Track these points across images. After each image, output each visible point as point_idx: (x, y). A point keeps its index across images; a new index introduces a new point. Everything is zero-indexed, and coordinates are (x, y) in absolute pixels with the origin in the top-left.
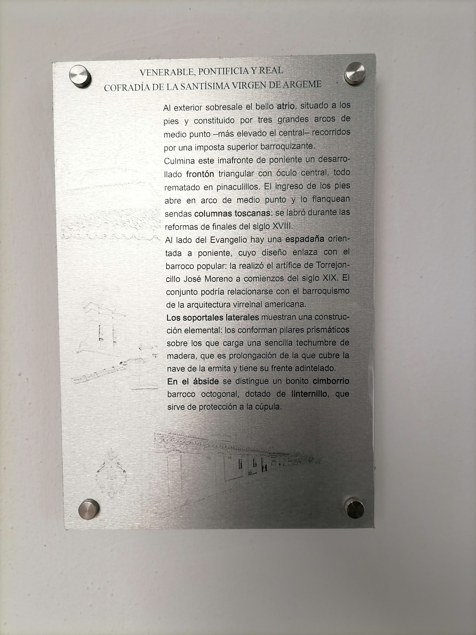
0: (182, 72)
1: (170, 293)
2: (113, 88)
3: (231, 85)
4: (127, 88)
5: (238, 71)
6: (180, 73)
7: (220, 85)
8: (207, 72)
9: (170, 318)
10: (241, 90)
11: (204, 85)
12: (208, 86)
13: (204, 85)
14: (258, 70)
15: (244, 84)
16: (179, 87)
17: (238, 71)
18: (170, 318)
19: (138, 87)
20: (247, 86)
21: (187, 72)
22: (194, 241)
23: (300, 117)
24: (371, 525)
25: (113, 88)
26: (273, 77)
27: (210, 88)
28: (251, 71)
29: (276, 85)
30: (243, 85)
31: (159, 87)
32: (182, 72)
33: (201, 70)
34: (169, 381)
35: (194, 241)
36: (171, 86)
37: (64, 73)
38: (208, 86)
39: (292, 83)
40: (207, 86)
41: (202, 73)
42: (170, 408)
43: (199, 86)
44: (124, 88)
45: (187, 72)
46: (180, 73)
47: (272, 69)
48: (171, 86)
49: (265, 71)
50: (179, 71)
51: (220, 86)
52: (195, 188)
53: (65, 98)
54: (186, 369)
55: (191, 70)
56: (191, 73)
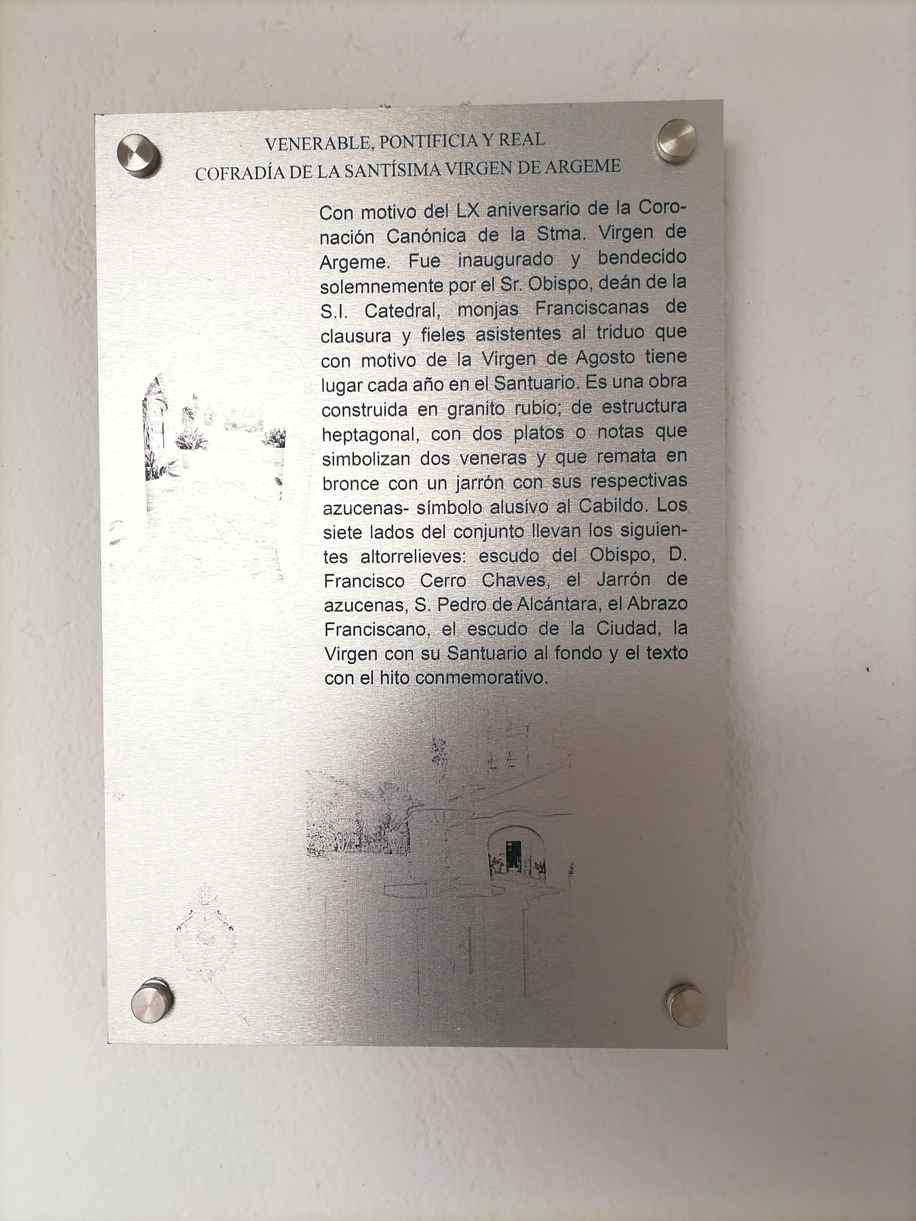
2: (213, 174)
4: (240, 175)
5: (456, 141)
11: (390, 170)
13: (390, 170)
14: (495, 140)
16: (342, 172)
17: (456, 141)
19: (261, 173)
21: (357, 142)
25: (213, 174)
29: (532, 167)
30: (467, 168)
31: (303, 172)
43: (381, 170)
44: (235, 174)
47: (523, 137)
51: (423, 170)
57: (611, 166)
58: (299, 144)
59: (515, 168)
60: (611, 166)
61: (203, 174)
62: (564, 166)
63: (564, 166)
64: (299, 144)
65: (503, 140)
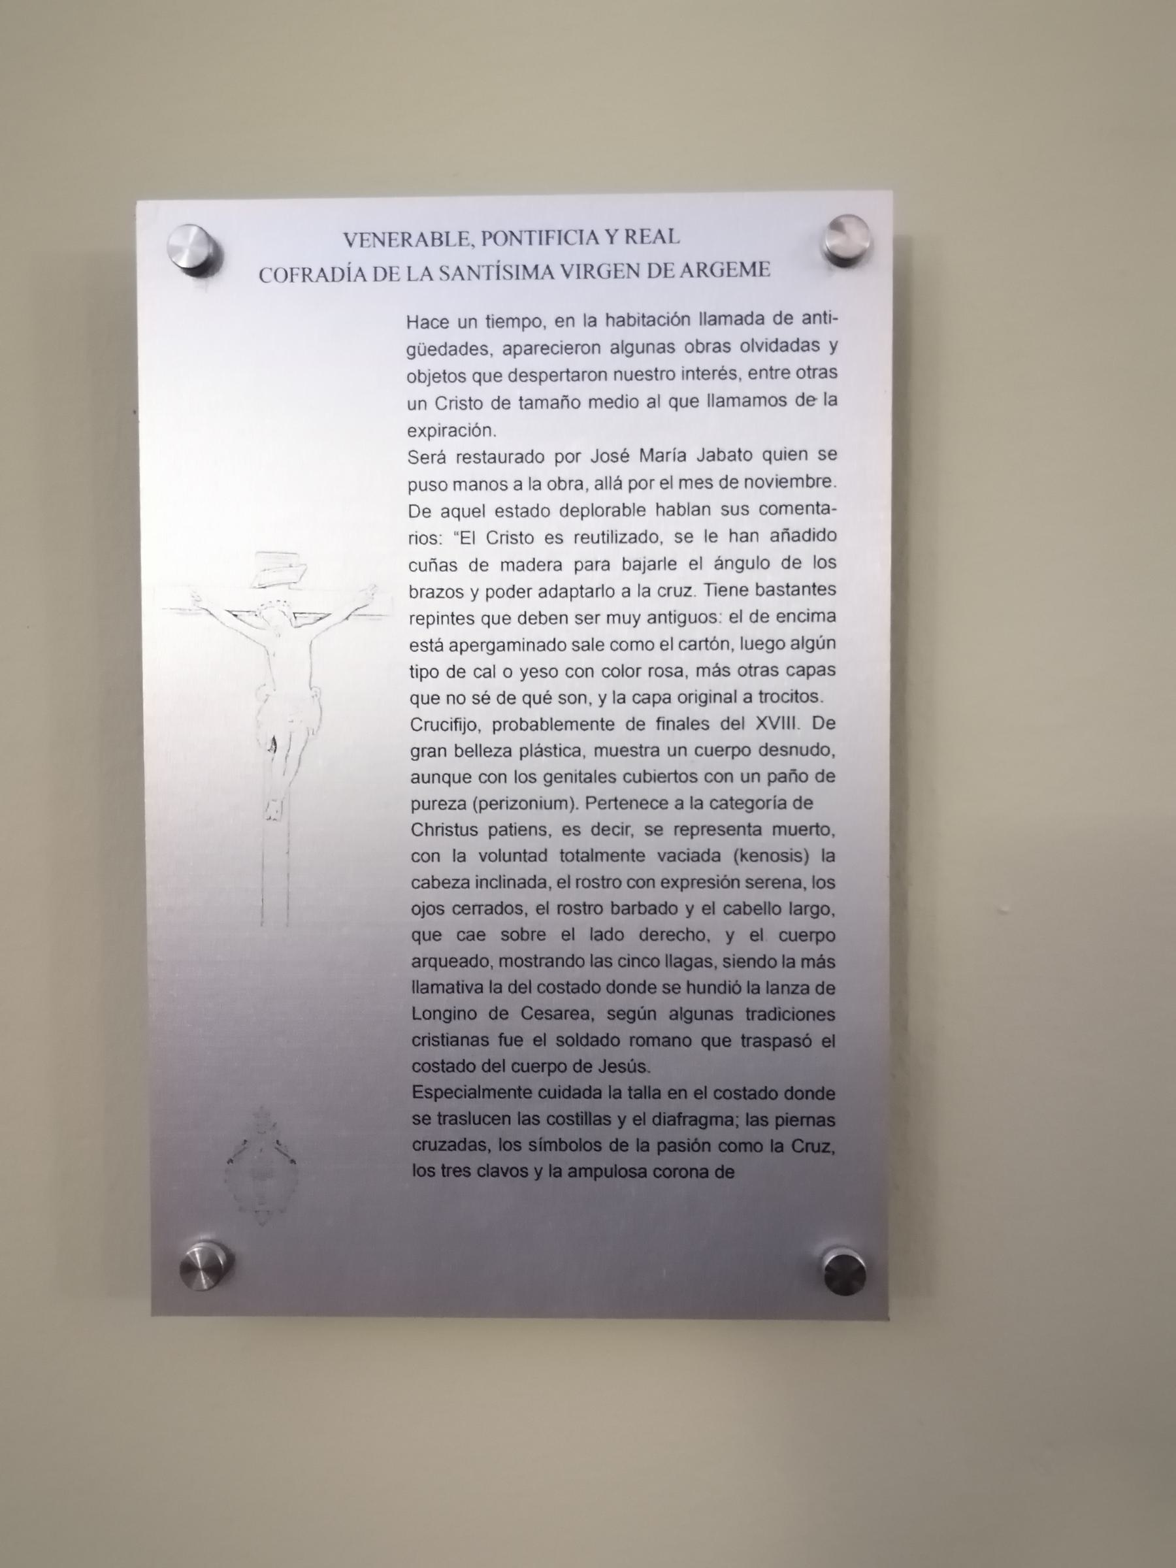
0: (444, 239)
1: (421, 1145)
3: (558, 272)
6: (437, 242)
7: (531, 269)
8: (500, 238)
9: (419, 1014)
10: (582, 281)
12: (500, 271)
13: (493, 271)
14: (620, 237)
15: (589, 268)
16: (436, 273)
18: (419, 1014)
20: (595, 272)
21: (454, 239)
22: (487, 404)
23: (499, 1009)
24: (880, 1313)
26: (659, 253)
27: (507, 276)
28: (604, 238)
31: (389, 274)
32: (444, 239)
33: (487, 235)
34: (415, 1091)
35: (487, 404)
36: (417, 272)
37: (162, 231)
38: (500, 271)
39: (702, 266)
40: (502, 273)
41: (490, 242)
42: (416, 1171)
43: (483, 272)
44: (306, 275)
45: (454, 239)
46: (437, 242)
48: (417, 272)
49: (638, 237)
50: (437, 236)
52: (476, 512)
53: (164, 305)
54: (505, 376)
55: (464, 235)
56: (464, 242)
57: (757, 269)
58: (386, 240)
59: (644, 271)
60: (757, 269)
61: (268, 275)
62: (703, 270)
63: (703, 270)
64: (386, 240)
65: (629, 236)
